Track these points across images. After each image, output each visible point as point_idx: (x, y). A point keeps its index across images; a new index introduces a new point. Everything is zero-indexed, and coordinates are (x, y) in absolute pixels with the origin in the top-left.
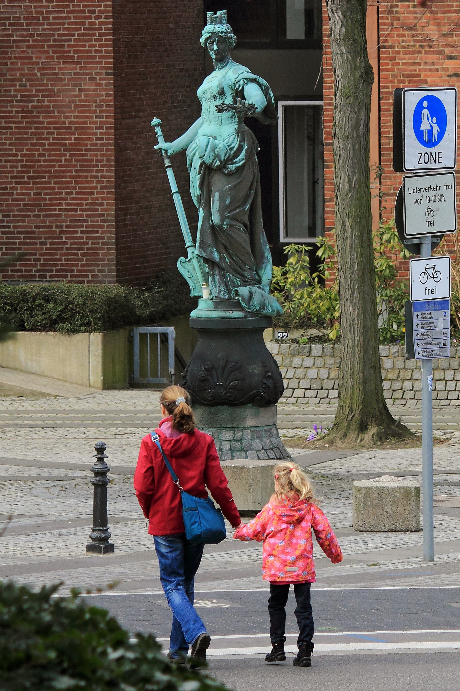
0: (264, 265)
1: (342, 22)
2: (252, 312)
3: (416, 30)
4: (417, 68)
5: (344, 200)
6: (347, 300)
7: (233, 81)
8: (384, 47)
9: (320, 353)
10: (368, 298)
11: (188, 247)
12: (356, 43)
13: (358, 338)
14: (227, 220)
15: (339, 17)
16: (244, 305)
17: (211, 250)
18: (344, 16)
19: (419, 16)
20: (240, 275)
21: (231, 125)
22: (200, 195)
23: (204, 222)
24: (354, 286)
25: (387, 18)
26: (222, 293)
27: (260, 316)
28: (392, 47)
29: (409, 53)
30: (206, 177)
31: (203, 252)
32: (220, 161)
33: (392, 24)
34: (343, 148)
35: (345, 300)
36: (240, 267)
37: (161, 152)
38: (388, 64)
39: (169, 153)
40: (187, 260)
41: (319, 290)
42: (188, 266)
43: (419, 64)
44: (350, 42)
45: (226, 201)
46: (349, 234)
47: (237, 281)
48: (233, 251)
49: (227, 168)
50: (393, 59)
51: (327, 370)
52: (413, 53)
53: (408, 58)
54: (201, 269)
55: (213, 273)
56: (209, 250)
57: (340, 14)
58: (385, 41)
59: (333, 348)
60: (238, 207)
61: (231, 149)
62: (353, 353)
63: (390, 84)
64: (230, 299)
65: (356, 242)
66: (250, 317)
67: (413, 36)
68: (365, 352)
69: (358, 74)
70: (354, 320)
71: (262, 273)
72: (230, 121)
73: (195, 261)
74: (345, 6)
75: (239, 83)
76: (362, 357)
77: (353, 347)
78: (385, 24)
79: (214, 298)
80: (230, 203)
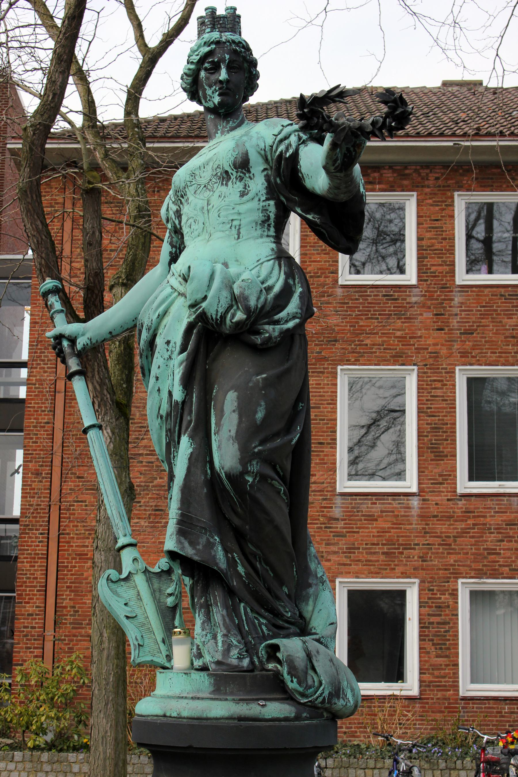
0: (311, 591)
1: (111, 438)
2: (312, 706)
3: (86, 522)
4: (86, 549)
5: (102, 611)
6: (100, 711)
7: (270, 140)
8: (63, 534)
9: (21, 759)
10: (121, 709)
11: (123, 547)
12: (122, 459)
13: (110, 750)
14: (254, 463)
15: (108, 433)
16: (292, 685)
17: (208, 539)
18: (113, 433)
19: (89, 512)
20: (267, 610)
21: (261, 240)
22: (184, 402)
23: (192, 469)
24: (108, 697)
25: (66, 514)
26: (234, 652)
27: (325, 714)
28: (69, 534)
29: (80, 538)
30: (201, 357)
31: (186, 544)
32: (247, 310)
33: (70, 518)
34: (105, 560)
35: (98, 711)
36: (269, 590)
37: (60, 344)
38: (65, 546)
39: (79, 345)
40: (123, 576)
41: (19, 708)
42: (123, 590)
43: (87, 546)
44: (117, 457)
45: (256, 412)
46: (106, 645)
47: (260, 624)
48: (257, 547)
49: (258, 333)
50: (68, 542)
51: (26, 773)
52: (84, 538)
53: (79, 542)
54: (154, 598)
55: (206, 601)
56: (203, 540)
57: (109, 431)
58: (64, 530)
59: (32, 755)
60: (277, 435)
61: (269, 289)
62: (105, 766)
63: (66, 561)
64: (252, 668)
65: (113, 653)
66: (306, 719)
67: (84, 526)
68: (116, 765)
69: (124, 488)
70: (106, 732)
71: (310, 608)
72: (259, 232)
73: (140, 580)
74: (114, 424)
75: (287, 142)
76: (112, 769)
77: (105, 759)
78: (64, 518)
79: (212, 667)
80: (265, 419)
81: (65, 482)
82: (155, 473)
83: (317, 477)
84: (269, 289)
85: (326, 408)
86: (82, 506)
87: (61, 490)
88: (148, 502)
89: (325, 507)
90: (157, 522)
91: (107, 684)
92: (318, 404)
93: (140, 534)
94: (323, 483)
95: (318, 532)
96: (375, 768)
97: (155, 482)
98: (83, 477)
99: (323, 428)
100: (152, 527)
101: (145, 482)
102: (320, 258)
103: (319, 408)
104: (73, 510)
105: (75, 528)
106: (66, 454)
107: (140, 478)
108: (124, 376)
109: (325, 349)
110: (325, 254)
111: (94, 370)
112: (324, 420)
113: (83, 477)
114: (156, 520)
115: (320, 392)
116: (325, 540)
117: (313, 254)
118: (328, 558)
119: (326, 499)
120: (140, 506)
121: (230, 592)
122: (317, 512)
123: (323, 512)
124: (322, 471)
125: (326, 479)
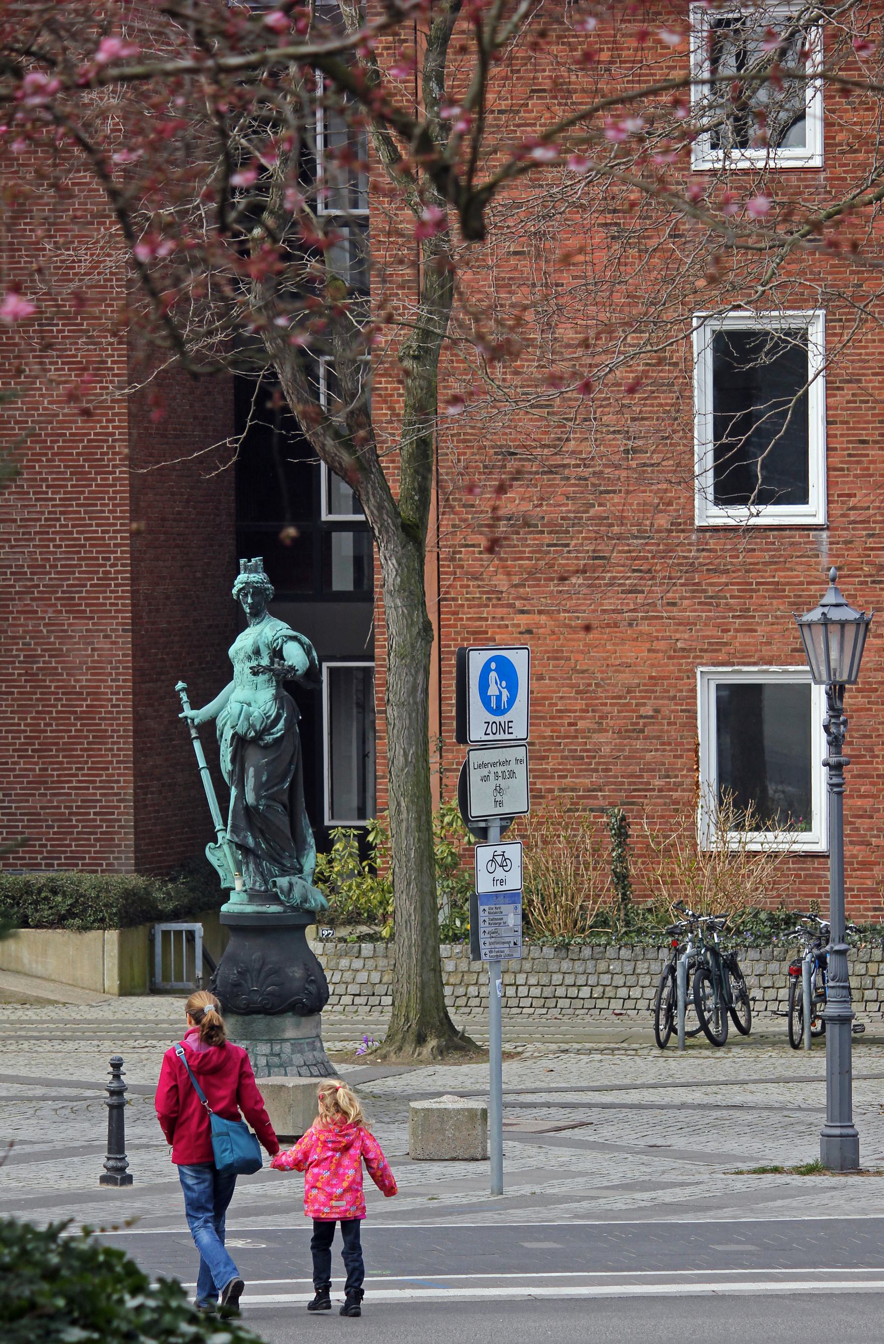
2: (292, 907)
3: (483, 580)
4: (484, 623)
8: (445, 599)
9: (371, 954)
16: (283, 898)
18: (399, 564)
25: (449, 567)
29: (474, 606)
32: (255, 731)
33: (455, 573)
38: (449, 620)
41: (370, 881)
42: (219, 854)
46: (404, 816)
50: (456, 613)
52: (480, 606)
53: (472, 613)
56: (242, 835)
57: (394, 561)
58: (447, 593)
59: (387, 948)
61: (268, 718)
62: (410, 954)
64: (266, 891)
65: (413, 824)
67: (479, 586)
68: (424, 953)
69: (415, 630)
70: (410, 916)
73: (226, 848)
77: (410, 947)
78: (446, 573)
80: (267, 780)
81: (444, 513)
82: (591, 497)
83: (857, 499)
84: (268, 718)
85: (871, 381)
86: (473, 552)
87: (438, 528)
88: (582, 545)
89: (872, 549)
90: (598, 578)
91: (408, 861)
92: (858, 375)
93: (570, 598)
94: (868, 508)
95: (861, 590)
96: (870, 961)
97: (592, 512)
98: (473, 506)
99: (867, 415)
100: (589, 586)
101: (574, 512)
102: (858, 116)
103: (859, 381)
104: (460, 559)
105: (464, 590)
106: (443, 467)
107: (567, 505)
108: (416, 484)
109: (867, 279)
110: (867, 110)
111: (368, 492)
112: (867, 402)
113: (473, 506)
114: (596, 575)
115: (860, 354)
116: (872, 603)
117: (846, 111)
118: (879, 632)
119: (872, 536)
120: (569, 552)
121: (257, 856)
122: (859, 556)
123: (869, 556)
124: (867, 489)
125: (873, 501)
